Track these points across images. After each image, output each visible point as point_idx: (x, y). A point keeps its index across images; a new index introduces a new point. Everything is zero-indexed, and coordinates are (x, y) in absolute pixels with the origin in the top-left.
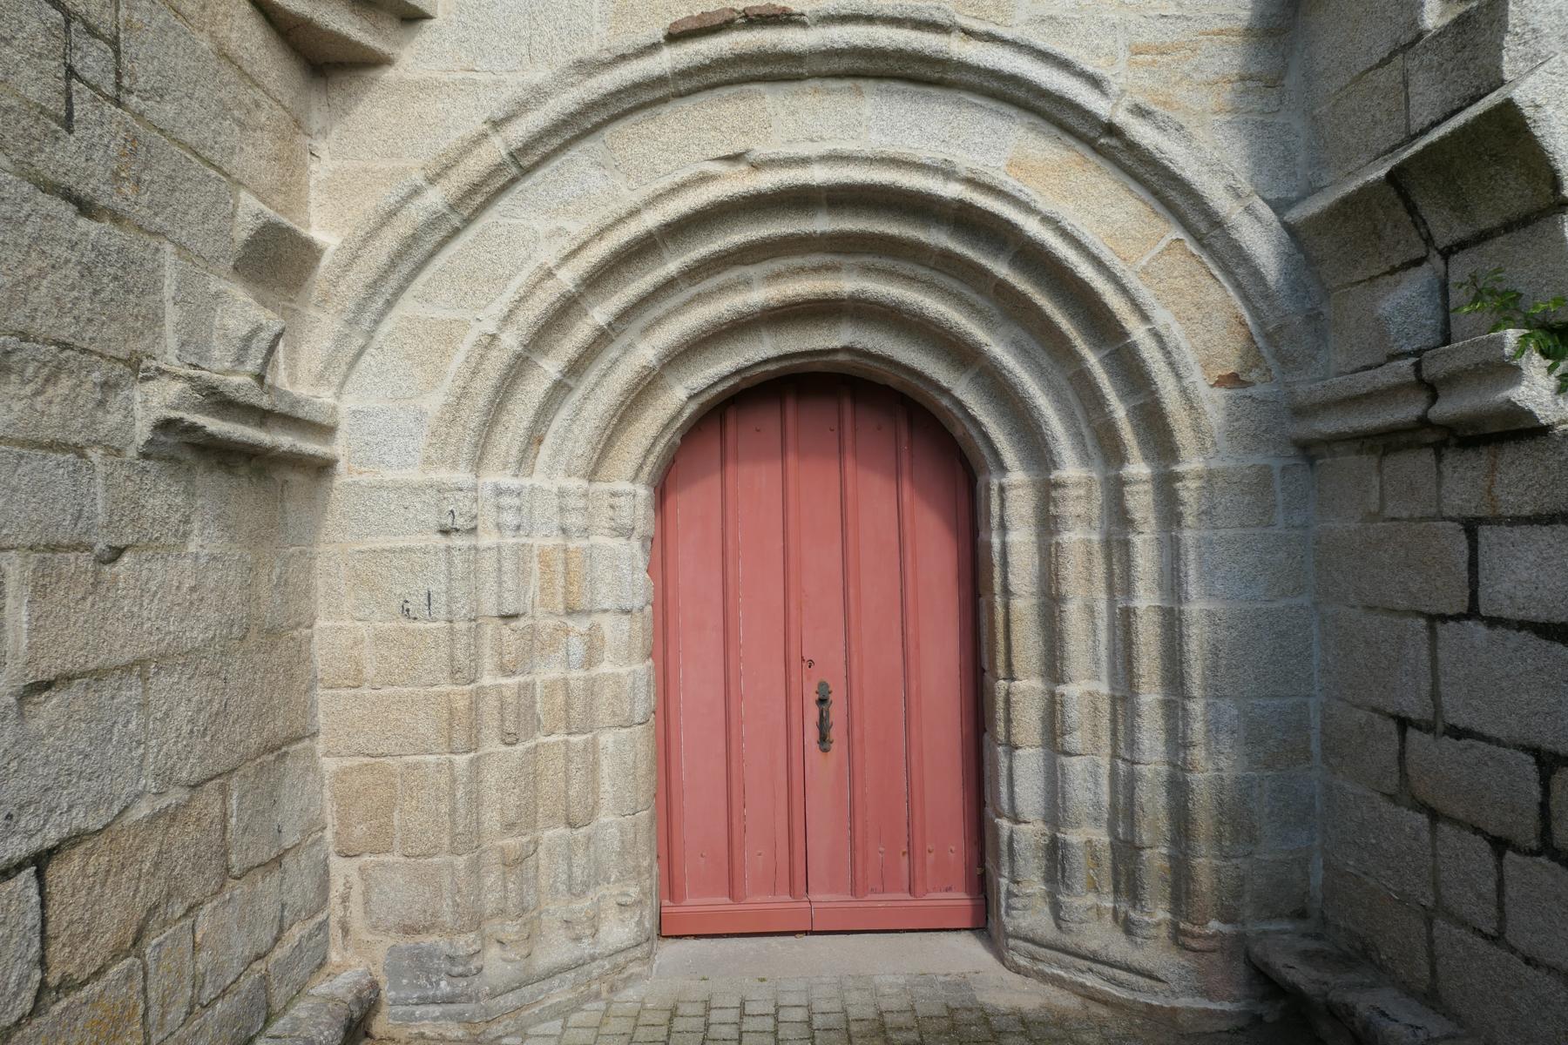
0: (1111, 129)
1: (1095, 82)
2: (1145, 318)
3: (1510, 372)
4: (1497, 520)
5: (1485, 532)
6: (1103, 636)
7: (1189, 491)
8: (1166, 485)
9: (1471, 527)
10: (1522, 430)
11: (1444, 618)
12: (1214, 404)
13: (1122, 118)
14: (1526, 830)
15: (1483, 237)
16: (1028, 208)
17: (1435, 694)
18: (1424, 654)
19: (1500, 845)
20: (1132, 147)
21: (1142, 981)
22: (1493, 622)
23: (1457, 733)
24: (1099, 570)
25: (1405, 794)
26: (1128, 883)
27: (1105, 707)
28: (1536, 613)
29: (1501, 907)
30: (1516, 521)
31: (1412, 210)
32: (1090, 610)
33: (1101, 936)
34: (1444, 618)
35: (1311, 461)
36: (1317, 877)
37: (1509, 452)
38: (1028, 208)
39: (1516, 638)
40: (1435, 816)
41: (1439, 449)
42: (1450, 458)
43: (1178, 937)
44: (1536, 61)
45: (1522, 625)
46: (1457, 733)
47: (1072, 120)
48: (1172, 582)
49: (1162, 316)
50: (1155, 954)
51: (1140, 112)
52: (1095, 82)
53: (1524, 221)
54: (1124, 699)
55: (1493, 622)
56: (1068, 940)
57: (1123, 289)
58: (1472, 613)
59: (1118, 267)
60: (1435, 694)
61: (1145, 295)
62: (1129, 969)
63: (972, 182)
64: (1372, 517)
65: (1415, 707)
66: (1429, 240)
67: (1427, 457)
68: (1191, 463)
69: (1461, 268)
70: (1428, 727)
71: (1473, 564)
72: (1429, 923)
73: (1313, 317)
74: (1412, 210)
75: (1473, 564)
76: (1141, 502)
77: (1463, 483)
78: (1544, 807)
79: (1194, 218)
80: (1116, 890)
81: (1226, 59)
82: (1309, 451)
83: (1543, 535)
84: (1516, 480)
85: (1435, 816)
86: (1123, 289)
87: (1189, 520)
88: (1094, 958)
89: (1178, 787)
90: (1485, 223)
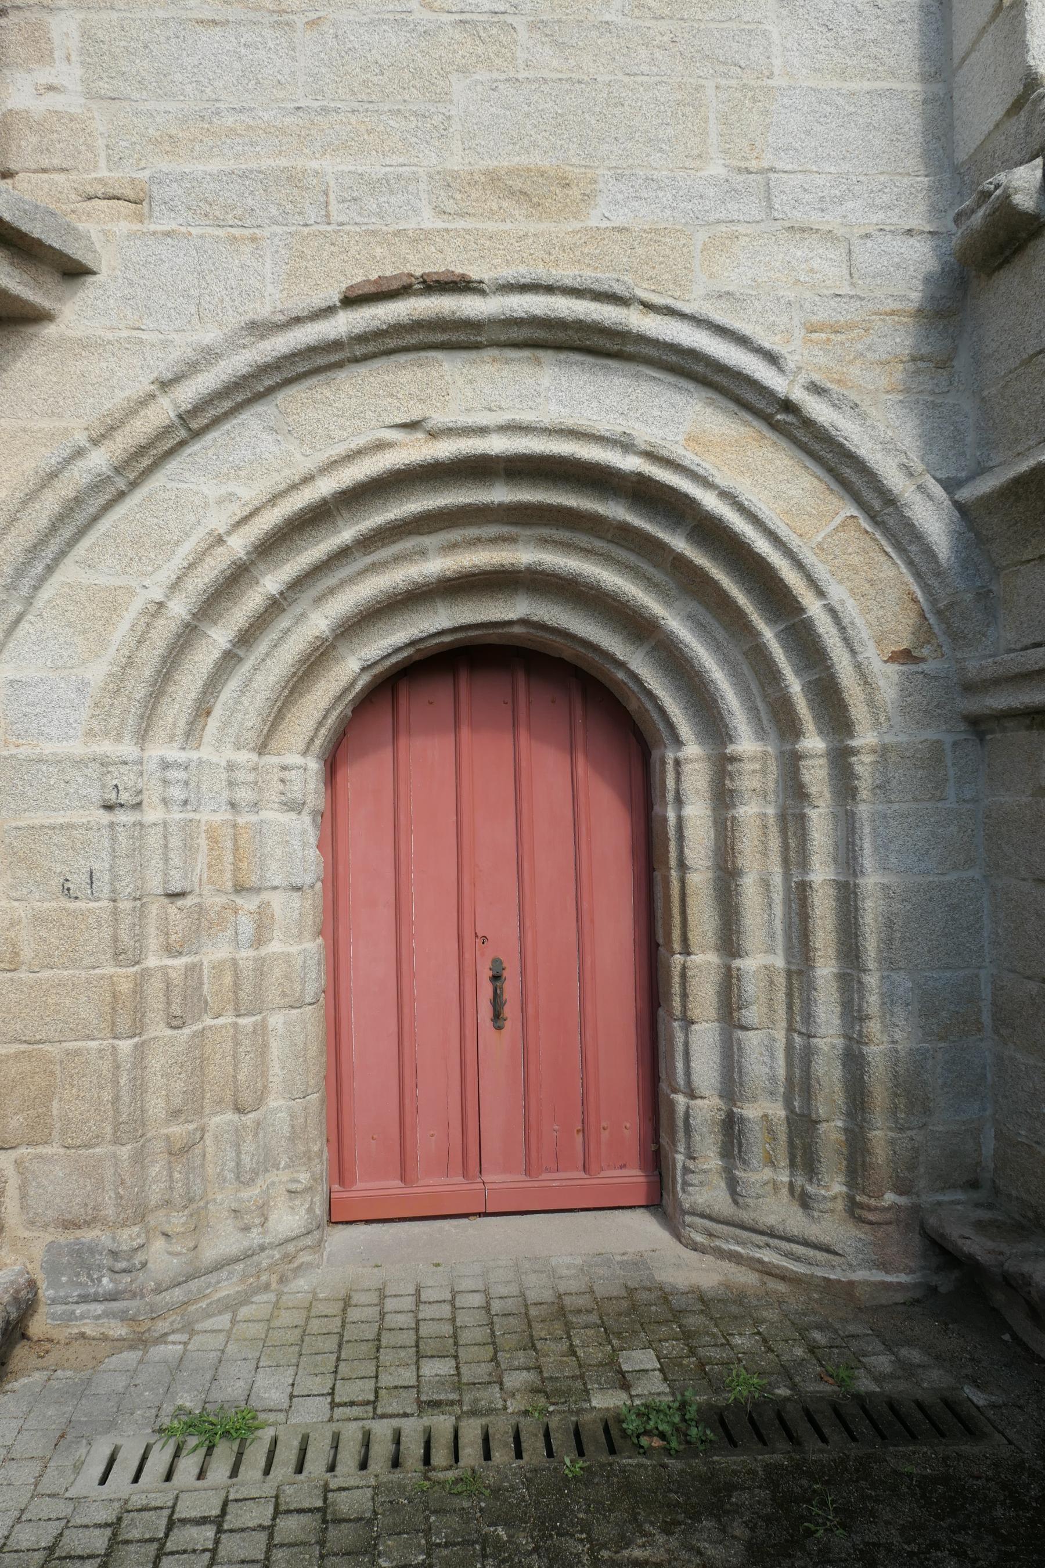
0: (788, 406)
1: (772, 358)
2: (821, 593)
6: (778, 910)
7: (863, 766)
8: (841, 759)
12: (887, 678)
13: (798, 395)
16: (706, 483)
20: (808, 423)
21: (819, 1255)
26: (803, 1155)
27: (781, 981)
28: (460, 1434)
33: (777, 1210)
36: (989, 1145)
38: (706, 483)
43: (854, 1210)
47: (749, 396)
48: (848, 856)
50: (831, 1227)
51: (816, 389)
52: (772, 358)
54: (800, 973)
56: (745, 1216)
57: (799, 565)
59: (794, 542)
61: (821, 572)
62: (806, 1243)
63: (651, 456)
79: (868, 495)
80: (792, 1165)
81: (898, 340)
82: (978, 726)
86: (799, 565)
89: (853, 1060)
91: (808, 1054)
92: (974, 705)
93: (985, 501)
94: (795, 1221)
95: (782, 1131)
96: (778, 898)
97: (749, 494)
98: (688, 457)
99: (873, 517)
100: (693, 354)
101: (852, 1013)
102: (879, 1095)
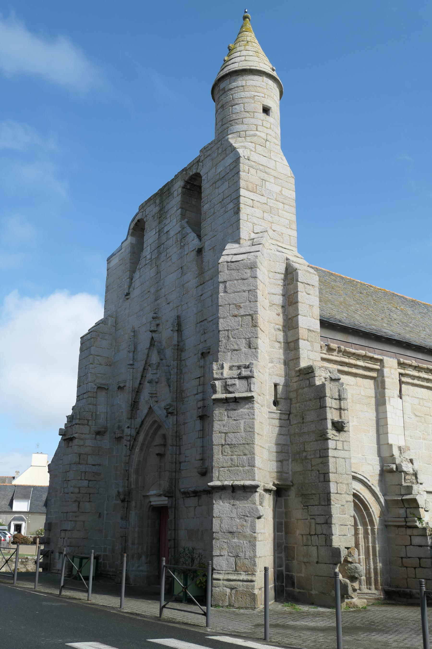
0: (370, 486)
1: (369, 481)
2: (371, 509)
3: (416, 522)
4: (413, 535)
5: (412, 537)
6: (364, 550)
7: (376, 530)
8: (373, 530)
9: (410, 536)
10: (416, 527)
11: (407, 546)
12: (378, 519)
13: (371, 485)
14: (418, 566)
15: (411, 508)
16: (361, 494)
17: (406, 554)
18: (405, 550)
19: (415, 568)
20: (372, 488)
21: (374, 595)
22: (413, 546)
23: (409, 558)
24: (363, 540)
25: (403, 566)
26: (368, 582)
27: (364, 559)
28: (418, 544)
29: (416, 575)
30: (415, 536)
31: (403, 503)
32: (362, 546)
33: (366, 591)
34: (407, 546)
35: (386, 527)
36: (389, 580)
37: (414, 529)
38: (361, 494)
39: (416, 547)
40: (407, 567)
41: (406, 528)
42: (407, 529)
43: (376, 589)
44: (205, 252)
45: (416, 546)
46: (409, 558)
47: (366, 484)
48: (374, 543)
49: (373, 508)
50: (374, 591)
51: (373, 484)
52: (369, 481)
53: (415, 508)
54: (367, 558)
55: (413, 546)
56: (363, 592)
57: (370, 505)
58: (411, 545)
59: (369, 502)
60: (406, 554)
61: (372, 506)
62: (372, 594)
63: (357, 491)
64: (397, 535)
65: (404, 555)
66: (404, 506)
67: (405, 528)
68: (376, 527)
69: (408, 510)
70: (406, 558)
71: (411, 540)
72: (407, 579)
73: (388, 510)
74: (403, 503)
75: (411, 540)
76: (370, 531)
77: (409, 532)
78: (420, 563)
79: (376, 497)
80: (367, 585)
81: (377, 478)
82: (386, 526)
83: (418, 537)
84: (415, 532)
85: (407, 567)
86: (370, 505)
87: (376, 534)
88: (367, 594)
89: (375, 569)
90: (411, 507)
91: (370, 568)
92: (387, 524)
93: (390, 500)
94: (370, 592)
95: (365, 580)
96: (364, 548)
97: (365, 496)
98: (360, 491)
99: (376, 500)
100: (362, 480)
101: (375, 563)
102: (379, 572)
